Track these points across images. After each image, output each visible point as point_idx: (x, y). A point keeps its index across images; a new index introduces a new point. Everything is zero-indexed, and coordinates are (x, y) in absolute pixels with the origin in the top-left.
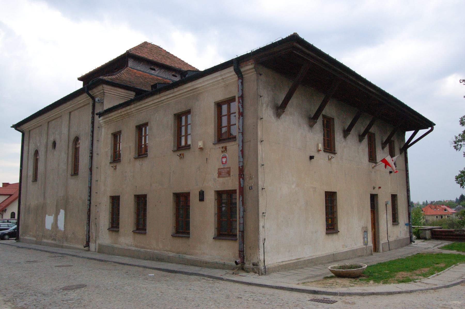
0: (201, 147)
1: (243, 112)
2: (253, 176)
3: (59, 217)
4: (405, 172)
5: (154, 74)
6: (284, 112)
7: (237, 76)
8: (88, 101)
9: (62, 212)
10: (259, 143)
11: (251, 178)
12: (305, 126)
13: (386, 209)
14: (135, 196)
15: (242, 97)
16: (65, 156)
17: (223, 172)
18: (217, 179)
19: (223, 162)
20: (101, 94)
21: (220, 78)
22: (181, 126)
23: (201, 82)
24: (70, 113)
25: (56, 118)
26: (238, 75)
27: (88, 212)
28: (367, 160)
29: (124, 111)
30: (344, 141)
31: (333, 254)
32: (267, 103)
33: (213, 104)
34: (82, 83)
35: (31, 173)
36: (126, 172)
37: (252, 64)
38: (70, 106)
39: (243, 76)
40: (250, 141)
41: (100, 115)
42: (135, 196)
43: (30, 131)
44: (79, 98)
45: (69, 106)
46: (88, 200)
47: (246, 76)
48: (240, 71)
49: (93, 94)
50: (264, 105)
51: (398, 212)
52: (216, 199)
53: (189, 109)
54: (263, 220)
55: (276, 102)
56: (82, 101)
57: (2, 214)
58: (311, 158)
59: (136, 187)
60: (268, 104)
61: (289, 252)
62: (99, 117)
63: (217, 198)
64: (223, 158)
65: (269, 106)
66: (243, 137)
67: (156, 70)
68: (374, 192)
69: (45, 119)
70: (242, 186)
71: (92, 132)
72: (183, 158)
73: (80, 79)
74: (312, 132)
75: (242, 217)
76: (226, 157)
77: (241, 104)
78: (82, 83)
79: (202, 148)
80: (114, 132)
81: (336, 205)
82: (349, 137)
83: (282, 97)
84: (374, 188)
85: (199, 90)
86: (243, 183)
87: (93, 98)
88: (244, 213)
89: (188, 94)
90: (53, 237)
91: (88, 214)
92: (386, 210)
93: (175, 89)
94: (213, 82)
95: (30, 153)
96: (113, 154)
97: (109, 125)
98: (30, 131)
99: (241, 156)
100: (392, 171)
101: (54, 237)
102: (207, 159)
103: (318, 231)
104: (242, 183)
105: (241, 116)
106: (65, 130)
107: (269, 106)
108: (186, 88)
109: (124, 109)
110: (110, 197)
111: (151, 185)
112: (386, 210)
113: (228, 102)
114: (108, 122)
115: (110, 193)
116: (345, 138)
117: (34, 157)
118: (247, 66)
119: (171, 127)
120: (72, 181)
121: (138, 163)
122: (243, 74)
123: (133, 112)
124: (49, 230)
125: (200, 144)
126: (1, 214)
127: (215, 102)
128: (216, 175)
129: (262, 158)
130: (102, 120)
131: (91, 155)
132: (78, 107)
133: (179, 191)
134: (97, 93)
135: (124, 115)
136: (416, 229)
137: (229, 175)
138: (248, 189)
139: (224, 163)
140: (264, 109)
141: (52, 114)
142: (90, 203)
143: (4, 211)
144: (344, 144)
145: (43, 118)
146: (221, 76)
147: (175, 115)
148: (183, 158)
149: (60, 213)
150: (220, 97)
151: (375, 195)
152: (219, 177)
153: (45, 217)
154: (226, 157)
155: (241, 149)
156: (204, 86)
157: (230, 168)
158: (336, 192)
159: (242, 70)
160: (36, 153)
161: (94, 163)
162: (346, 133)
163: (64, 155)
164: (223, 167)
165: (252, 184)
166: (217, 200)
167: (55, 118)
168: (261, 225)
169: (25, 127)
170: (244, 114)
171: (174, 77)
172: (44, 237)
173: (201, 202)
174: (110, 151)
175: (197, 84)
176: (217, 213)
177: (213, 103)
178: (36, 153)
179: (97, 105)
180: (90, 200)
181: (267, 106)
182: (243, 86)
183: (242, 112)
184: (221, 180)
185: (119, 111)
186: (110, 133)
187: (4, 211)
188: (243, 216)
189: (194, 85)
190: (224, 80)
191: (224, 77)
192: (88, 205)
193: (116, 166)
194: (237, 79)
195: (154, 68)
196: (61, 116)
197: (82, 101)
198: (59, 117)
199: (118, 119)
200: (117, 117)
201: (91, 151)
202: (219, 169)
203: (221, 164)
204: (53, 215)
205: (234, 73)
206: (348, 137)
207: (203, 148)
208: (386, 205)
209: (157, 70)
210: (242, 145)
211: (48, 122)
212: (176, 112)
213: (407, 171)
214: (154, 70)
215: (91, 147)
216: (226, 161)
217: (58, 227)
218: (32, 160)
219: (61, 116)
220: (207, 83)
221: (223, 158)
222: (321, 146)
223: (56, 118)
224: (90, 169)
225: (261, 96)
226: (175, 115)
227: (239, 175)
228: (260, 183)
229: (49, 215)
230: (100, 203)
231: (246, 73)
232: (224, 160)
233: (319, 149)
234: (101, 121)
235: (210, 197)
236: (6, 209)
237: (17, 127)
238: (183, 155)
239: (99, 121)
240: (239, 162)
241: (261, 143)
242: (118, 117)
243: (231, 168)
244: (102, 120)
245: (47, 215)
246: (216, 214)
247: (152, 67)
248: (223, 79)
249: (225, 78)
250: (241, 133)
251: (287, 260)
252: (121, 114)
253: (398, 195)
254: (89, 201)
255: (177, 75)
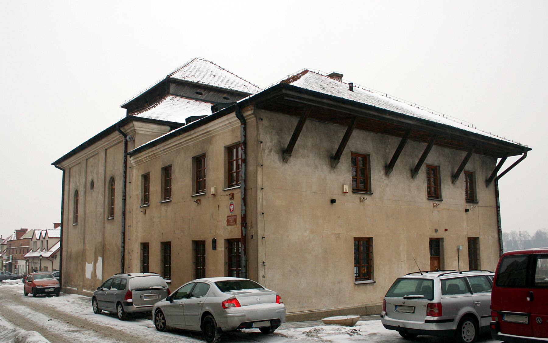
0: (213, 193)
1: (245, 159)
2: (254, 225)
3: (97, 264)
4: (494, 210)
5: (201, 98)
6: (291, 156)
7: (239, 121)
8: (121, 138)
9: (100, 259)
10: (259, 191)
11: (252, 227)
12: (325, 167)
13: (458, 256)
14: (162, 243)
15: (245, 143)
16: (102, 197)
17: (231, 219)
18: (226, 227)
19: (231, 209)
20: (132, 132)
21: (227, 122)
22: (233, 160)
23: (212, 126)
24: (106, 150)
25: (94, 156)
26: (240, 120)
27: (122, 260)
28: (424, 197)
29: (151, 152)
30: (385, 179)
31: (366, 307)
32: (270, 148)
33: (223, 149)
34: (125, 110)
35: (71, 216)
36: (154, 217)
37: (251, 109)
38: (106, 142)
39: (245, 121)
40: (251, 188)
41: (133, 154)
42: (162, 243)
43: (70, 168)
44: (112, 135)
45: (104, 143)
46: (122, 247)
47: (248, 121)
48: (243, 116)
49: (125, 132)
50: (266, 151)
51: (480, 257)
52: (226, 248)
53: (204, 152)
54: (263, 269)
55: (282, 145)
56: (115, 138)
57: (52, 260)
58: (333, 201)
59: (162, 233)
60: (271, 150)
61: (299, 303)
62: (130, 157)
63: (227, 247)
64: (231, 205)
65: (273, 151)
66: (245, 184)
67: (203, 94)
68: (436, 236)
69: (83, 156)
70: (244, 235)
71: (124, 173)
72: (199, 204)
73: (123, 107)
74: (334, 172)
75: (244, 267)
76: (233, 204)
77: (243, 151)
78: (125, 110)
79: (214, 194)
80: (144, 173)
81: (372, 252)
82: (394, 173)
83: (288, 139)
84: (436, 231)
85: (211, 134)
86: (246, 231)
87: (125, 135)
88: (246, 263)
89: (203, 137)
90: (92, 287)
91: (122, 262)
92: (458, 257)
93: (192, 131)
94: (222, 126)
95: (71, 193)
96: (143, 198)
97: (139, 165)
98: (70, 168)
99: (243, 204)
100: (468, 210)
101: (93, 287)
102: (218, 206)
103: (342, 282)
104: (244, 232)
105: (243, 163)
106: (101, 170)
107: (273, 151)
108: (200, 131)
109: (150, 150)
110: (141, 243)
111: (174, 232)
112: (458, 257)
113: (236, 147)
114: (138, 163)
115: (140, 240)
116: (388, 176)
117: (74, 198)
118: (247, 111)
119: (190, 171)
120: (108, 226)
121: (163, 208)
122: (245, 119)
123: (159, 153)
124: (89, 279)
125: (213, 190)
126: (51, 261)
127: (224, 147)
128: (225, 223)
129: (262, 206)
130: (133, 160)
131: (124, 198)
132: (112, 144)
133: (197, 239)
134: (129, 130)
135: (151, 156)
136: (460, 281)
137: (236, 222)
138: (250, 238)
139: (232, 210)
140: (266, 155)
141: (90, 151)
142: (124, 250)
143: (54, 257)
144: (386, 181)
145: (80, 155)
146: (228, 120)
147: (193, 158)
148: (199, 204)
149: (98, 261)
150: (229, 142)
151: (440, 240)
152: (228, 225)
153: (85, 264)
154: (233, 204)
155: (243, 196)
156: (215, 129)
157: (236, 216)
158: (372, 238)
159: (245, 114)
160: (77, 193)
161: (127, 207)
162: (389, 168)
163: (101, 197)
164: (230, 215)
165: (253, 233)
166: (227, 249)
167: (93, 155)
168: (261, 274)
169: (65, 163)
170: (247, 161)
171: (226, 100)
172: (84, 287)
173: (214, 251)
174: (140, 193)
175: (209, 127)
176: (227, 262)
177: (223, 147)
178: (77, 193)
179: (129, 144)
180: (124, 247)
181: (270, 151)
182: (246, 132)
183: (244, 159)
184: (229, 227)
185: (147, 151)
186: (141, 175)
187: (54, 257)
188: (245, 266)
189: (208, 127)
190: (231, 124)
191: (230, 121)
192: (122, 252)
193: (145, 211)
194: (240, 124)
195: (201, 92)
196: (98, 153)
197: (115, 138)
198: (96, 155)
199: (147, 159)
200: (146, 157)
201: (124, 194)
202: (228, 217)
203: (229, 211)
204: (92, 263)
205: (237, 118)
206: (393, 174)
207: (215, 194)
208: (458, 250)
209: (205, 94)
210: (244, 193)
211: (87, 160)
212: (194, 155)
213: (498, 207)
214: (201, 94)
215: (124, 190)
216: (233, 209)
217: (96, 276)
218: (72, 202)
219: (98, 153)
220: (217, 126)
221: (231, 205)
222: (346, 188)
223: (94, 156)
224: (123, 214)
225: (261, 142)
226: (193, 158)
227: (241, 223)
228: (260, 232)
229: (89, 263)
230: (133, 251)
231: (247, 118)
232: (232, 207)
233: (345, 191)
234: (132, 162)
235: (221, 247)
236: (56, 255)
237: (57, 164)
238: (200, 200)
239: (130, 161)
240: (242, 210)
241: (261, 191)
242: (147, 158)
243: (237, 216)
244: (133, 160)
245: (87, 263)
246: (226, 263)
247: (198, 91)
248: (230, 123)
249: (232, 122)
250: (243, 181)
251: (306, 310)
252: (149, 155)
253: (481, 237)
254: (122, 248)
255: (229, 97)
